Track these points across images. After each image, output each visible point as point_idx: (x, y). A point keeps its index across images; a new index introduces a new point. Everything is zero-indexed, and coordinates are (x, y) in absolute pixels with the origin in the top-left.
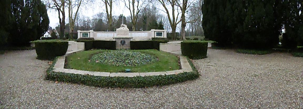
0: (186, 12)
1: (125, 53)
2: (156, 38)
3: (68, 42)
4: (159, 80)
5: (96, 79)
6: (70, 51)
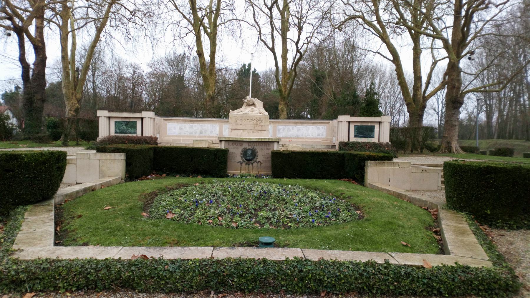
0: (465, 55)
1: (258, 187)
2: (354, 143)
3: (64, 154)
4: (367, 278)
5: (169, 270)
6: (70, 185)
